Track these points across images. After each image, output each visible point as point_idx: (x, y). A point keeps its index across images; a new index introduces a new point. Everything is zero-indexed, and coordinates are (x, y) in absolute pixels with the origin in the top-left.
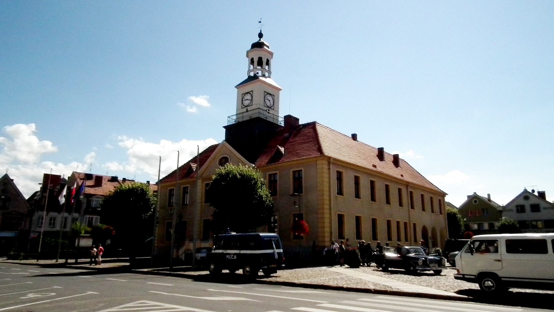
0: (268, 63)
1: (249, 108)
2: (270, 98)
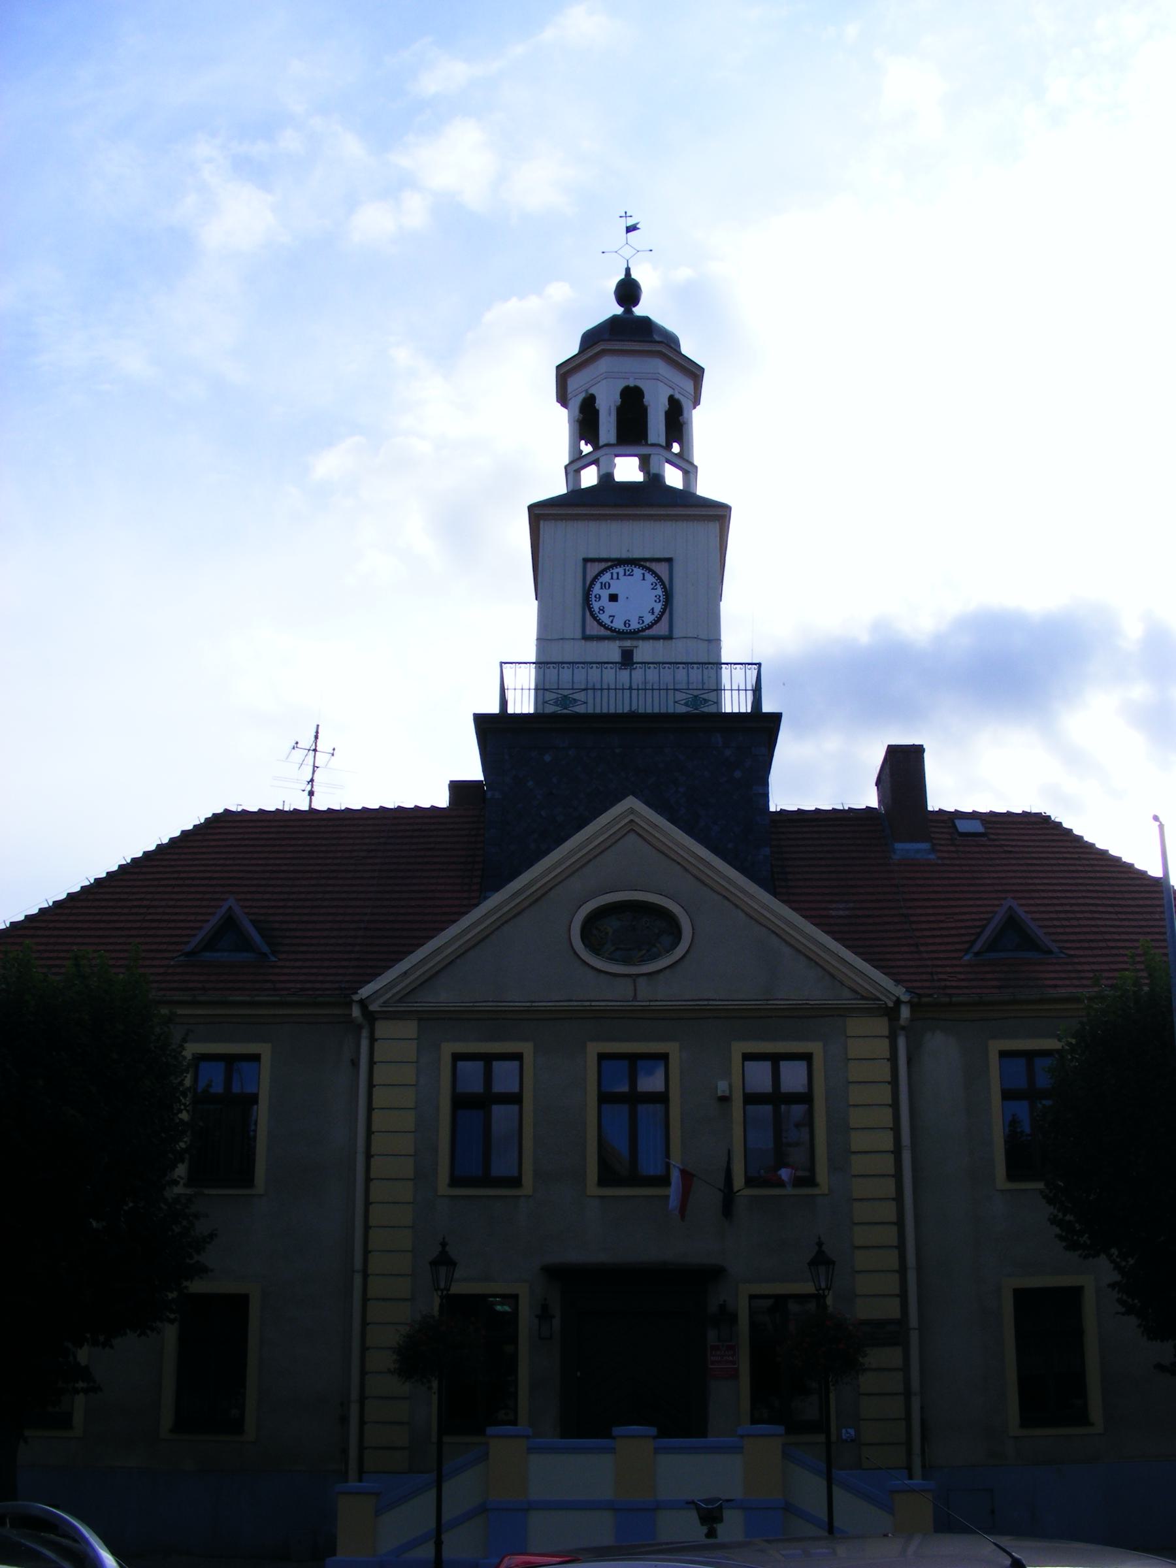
0: (677, 424)
1: (644, 651)
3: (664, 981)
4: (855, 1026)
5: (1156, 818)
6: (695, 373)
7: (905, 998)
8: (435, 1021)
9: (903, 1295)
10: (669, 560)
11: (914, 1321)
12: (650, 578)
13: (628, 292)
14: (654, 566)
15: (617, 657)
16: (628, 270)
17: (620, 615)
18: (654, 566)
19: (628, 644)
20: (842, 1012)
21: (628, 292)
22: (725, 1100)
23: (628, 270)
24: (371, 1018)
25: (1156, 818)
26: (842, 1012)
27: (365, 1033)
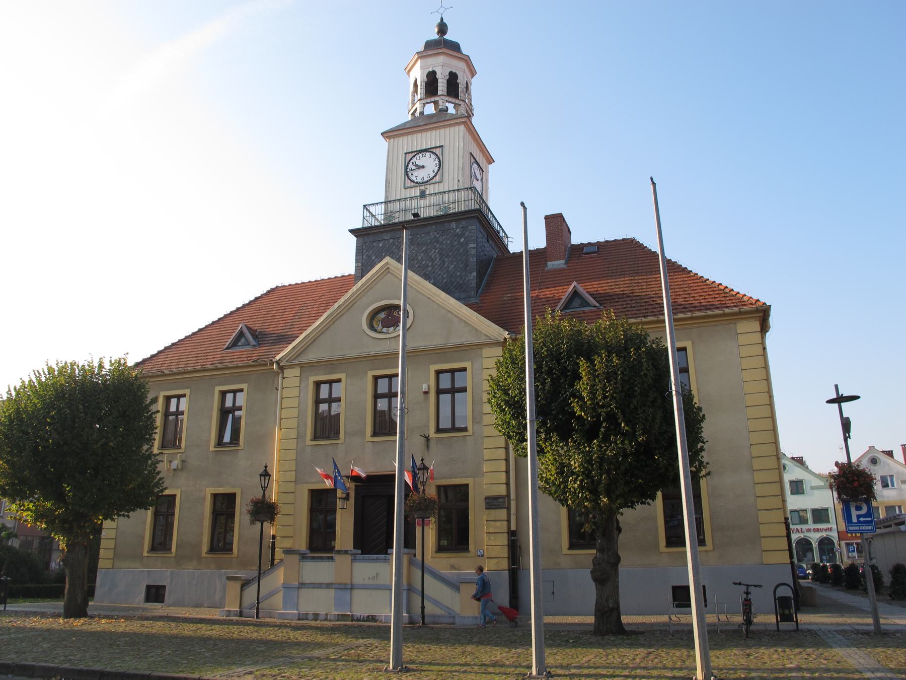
1: (430, 189)
3: (397, 340)
4: (486, 352)
5: (522, 204)
7: (507, 337)
8: (306, 368)
9: (508, 484)
10: (441, 146)
11: (513, 496)
12: (433, 156)
13: (442, 28)
14: (434, 150)
15: (418, 194)
16: (442, 19)
17: (419, 176)
18: (434, 150)
19: (423, 188)
20: (481, 346)
21: (442, 28)
22: (426, 393)
23: (442, 19)
24: (282, 368)
25: (522, 204)
26: (481, 346)
27: (280, 376)
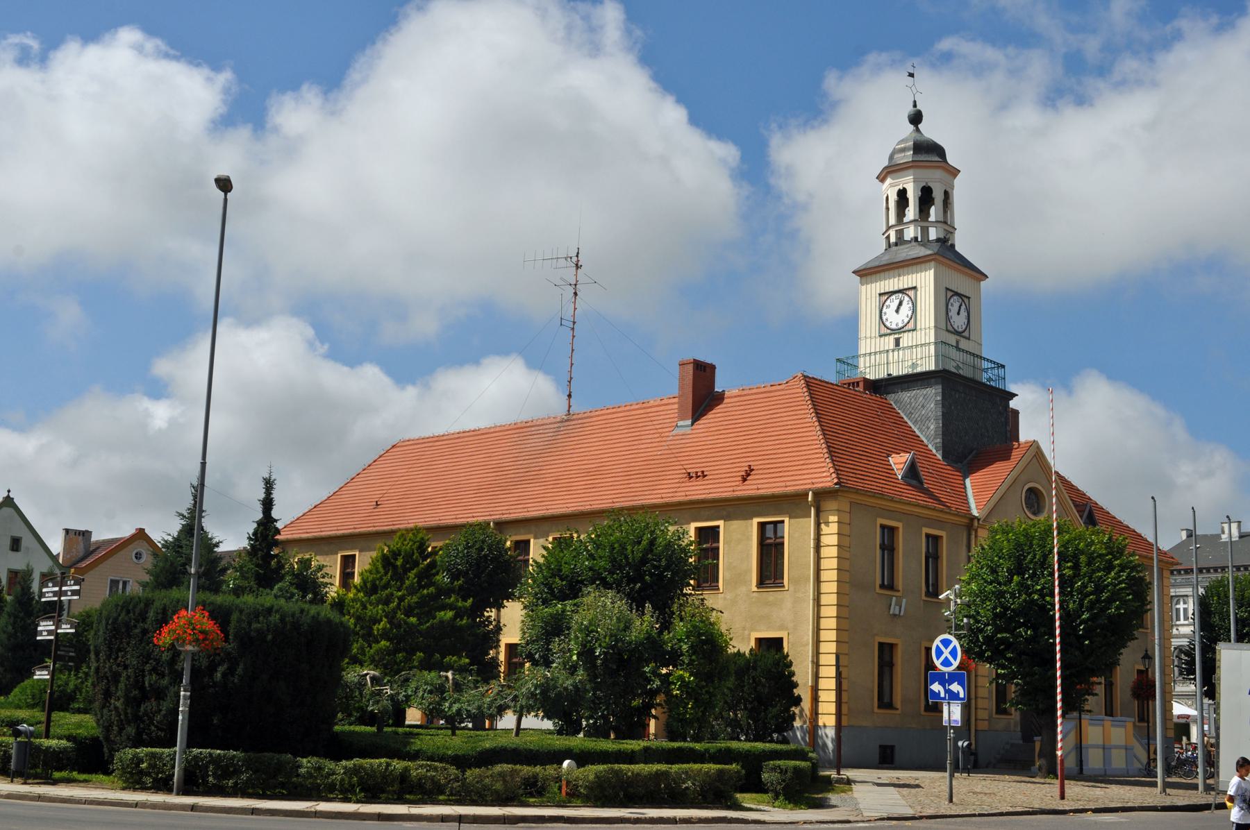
1: (906, 340)
2: (955, 302)
6: (954, 172)
